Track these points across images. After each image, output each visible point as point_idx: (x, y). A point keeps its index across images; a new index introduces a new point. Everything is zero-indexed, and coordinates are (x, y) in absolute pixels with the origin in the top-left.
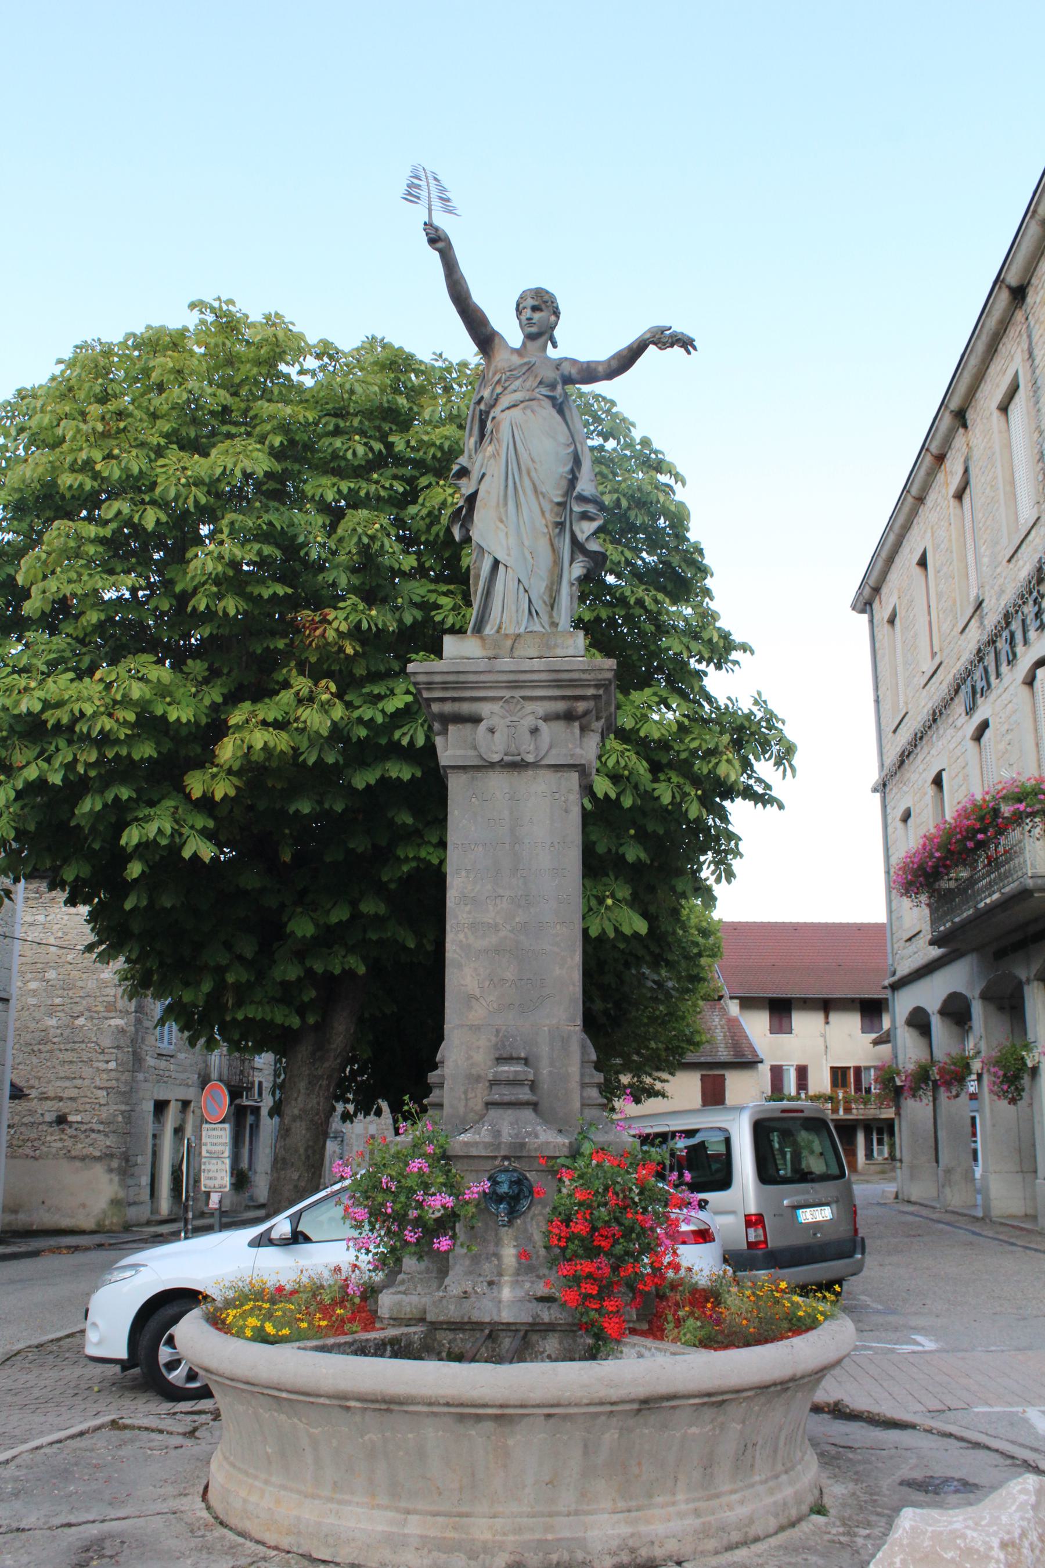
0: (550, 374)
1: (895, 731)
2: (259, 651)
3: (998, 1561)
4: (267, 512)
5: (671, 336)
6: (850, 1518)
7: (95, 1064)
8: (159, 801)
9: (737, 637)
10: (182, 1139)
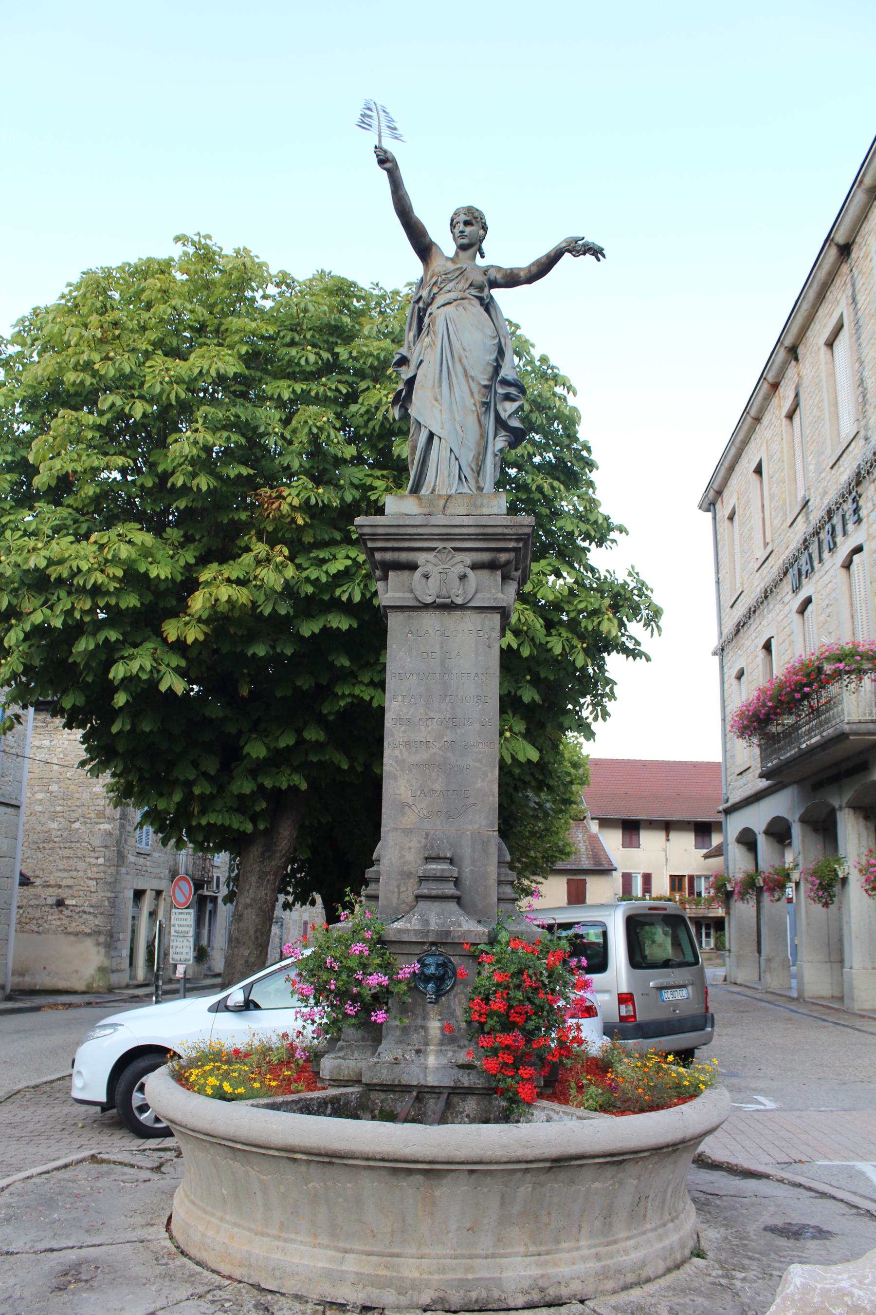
0: (480, 279)
1: (732, 607)
2: (225, 521)
4: (234, 406)
5: (584, 245)
7: (88, 860)
8: (141, 644)
9: (615, 521)
10: (155, 921)
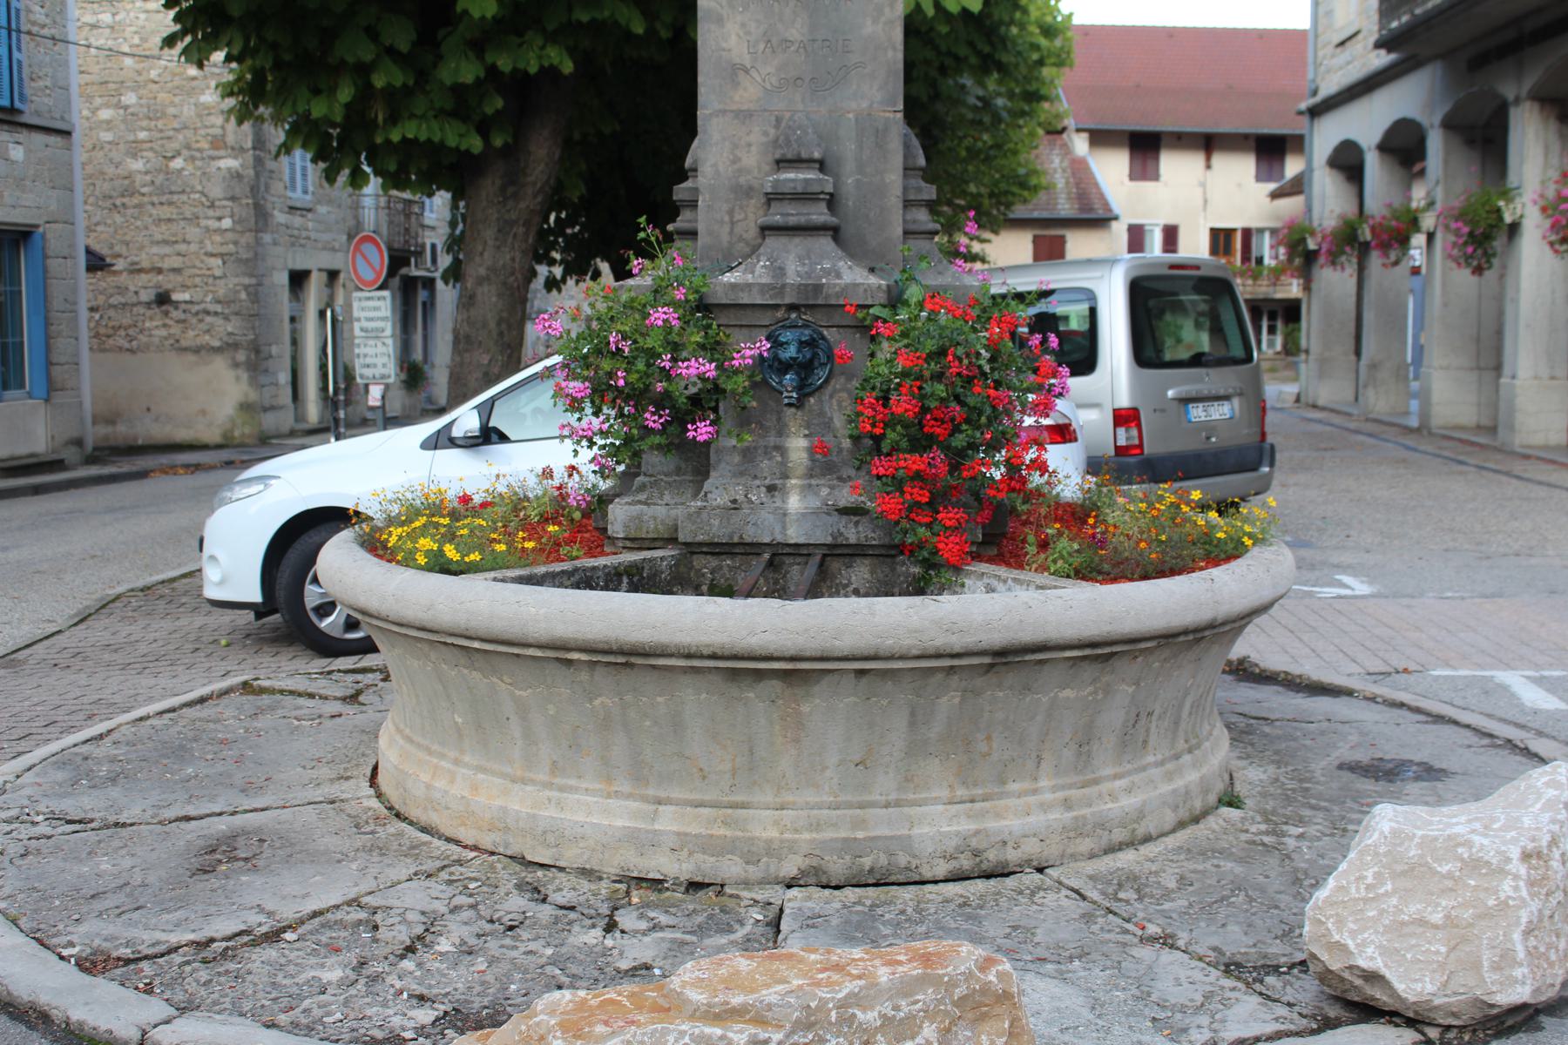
3: (1516, 877)
6: (1274, 812)
7: (203, 222)
